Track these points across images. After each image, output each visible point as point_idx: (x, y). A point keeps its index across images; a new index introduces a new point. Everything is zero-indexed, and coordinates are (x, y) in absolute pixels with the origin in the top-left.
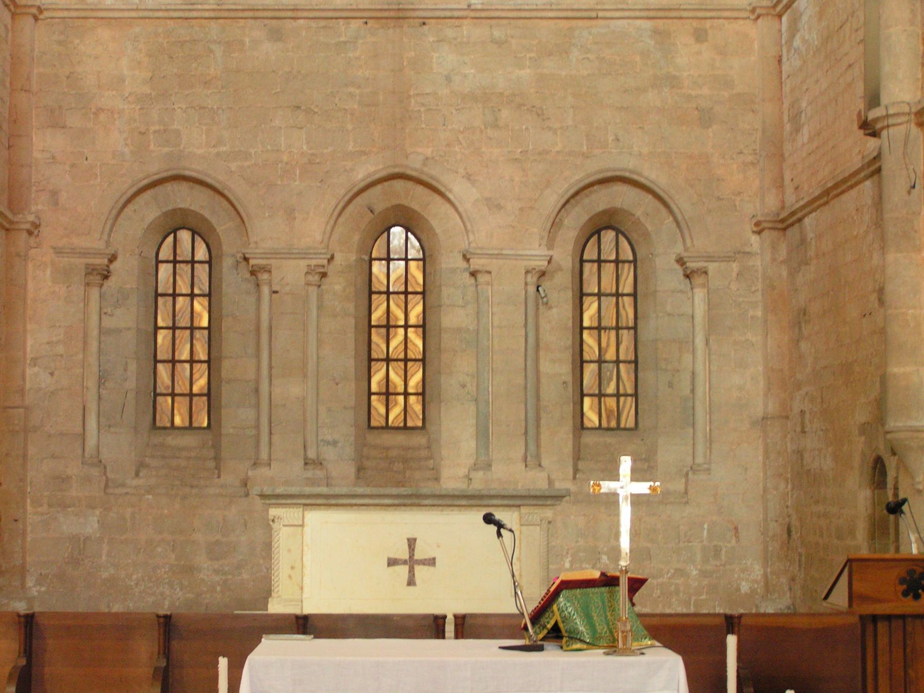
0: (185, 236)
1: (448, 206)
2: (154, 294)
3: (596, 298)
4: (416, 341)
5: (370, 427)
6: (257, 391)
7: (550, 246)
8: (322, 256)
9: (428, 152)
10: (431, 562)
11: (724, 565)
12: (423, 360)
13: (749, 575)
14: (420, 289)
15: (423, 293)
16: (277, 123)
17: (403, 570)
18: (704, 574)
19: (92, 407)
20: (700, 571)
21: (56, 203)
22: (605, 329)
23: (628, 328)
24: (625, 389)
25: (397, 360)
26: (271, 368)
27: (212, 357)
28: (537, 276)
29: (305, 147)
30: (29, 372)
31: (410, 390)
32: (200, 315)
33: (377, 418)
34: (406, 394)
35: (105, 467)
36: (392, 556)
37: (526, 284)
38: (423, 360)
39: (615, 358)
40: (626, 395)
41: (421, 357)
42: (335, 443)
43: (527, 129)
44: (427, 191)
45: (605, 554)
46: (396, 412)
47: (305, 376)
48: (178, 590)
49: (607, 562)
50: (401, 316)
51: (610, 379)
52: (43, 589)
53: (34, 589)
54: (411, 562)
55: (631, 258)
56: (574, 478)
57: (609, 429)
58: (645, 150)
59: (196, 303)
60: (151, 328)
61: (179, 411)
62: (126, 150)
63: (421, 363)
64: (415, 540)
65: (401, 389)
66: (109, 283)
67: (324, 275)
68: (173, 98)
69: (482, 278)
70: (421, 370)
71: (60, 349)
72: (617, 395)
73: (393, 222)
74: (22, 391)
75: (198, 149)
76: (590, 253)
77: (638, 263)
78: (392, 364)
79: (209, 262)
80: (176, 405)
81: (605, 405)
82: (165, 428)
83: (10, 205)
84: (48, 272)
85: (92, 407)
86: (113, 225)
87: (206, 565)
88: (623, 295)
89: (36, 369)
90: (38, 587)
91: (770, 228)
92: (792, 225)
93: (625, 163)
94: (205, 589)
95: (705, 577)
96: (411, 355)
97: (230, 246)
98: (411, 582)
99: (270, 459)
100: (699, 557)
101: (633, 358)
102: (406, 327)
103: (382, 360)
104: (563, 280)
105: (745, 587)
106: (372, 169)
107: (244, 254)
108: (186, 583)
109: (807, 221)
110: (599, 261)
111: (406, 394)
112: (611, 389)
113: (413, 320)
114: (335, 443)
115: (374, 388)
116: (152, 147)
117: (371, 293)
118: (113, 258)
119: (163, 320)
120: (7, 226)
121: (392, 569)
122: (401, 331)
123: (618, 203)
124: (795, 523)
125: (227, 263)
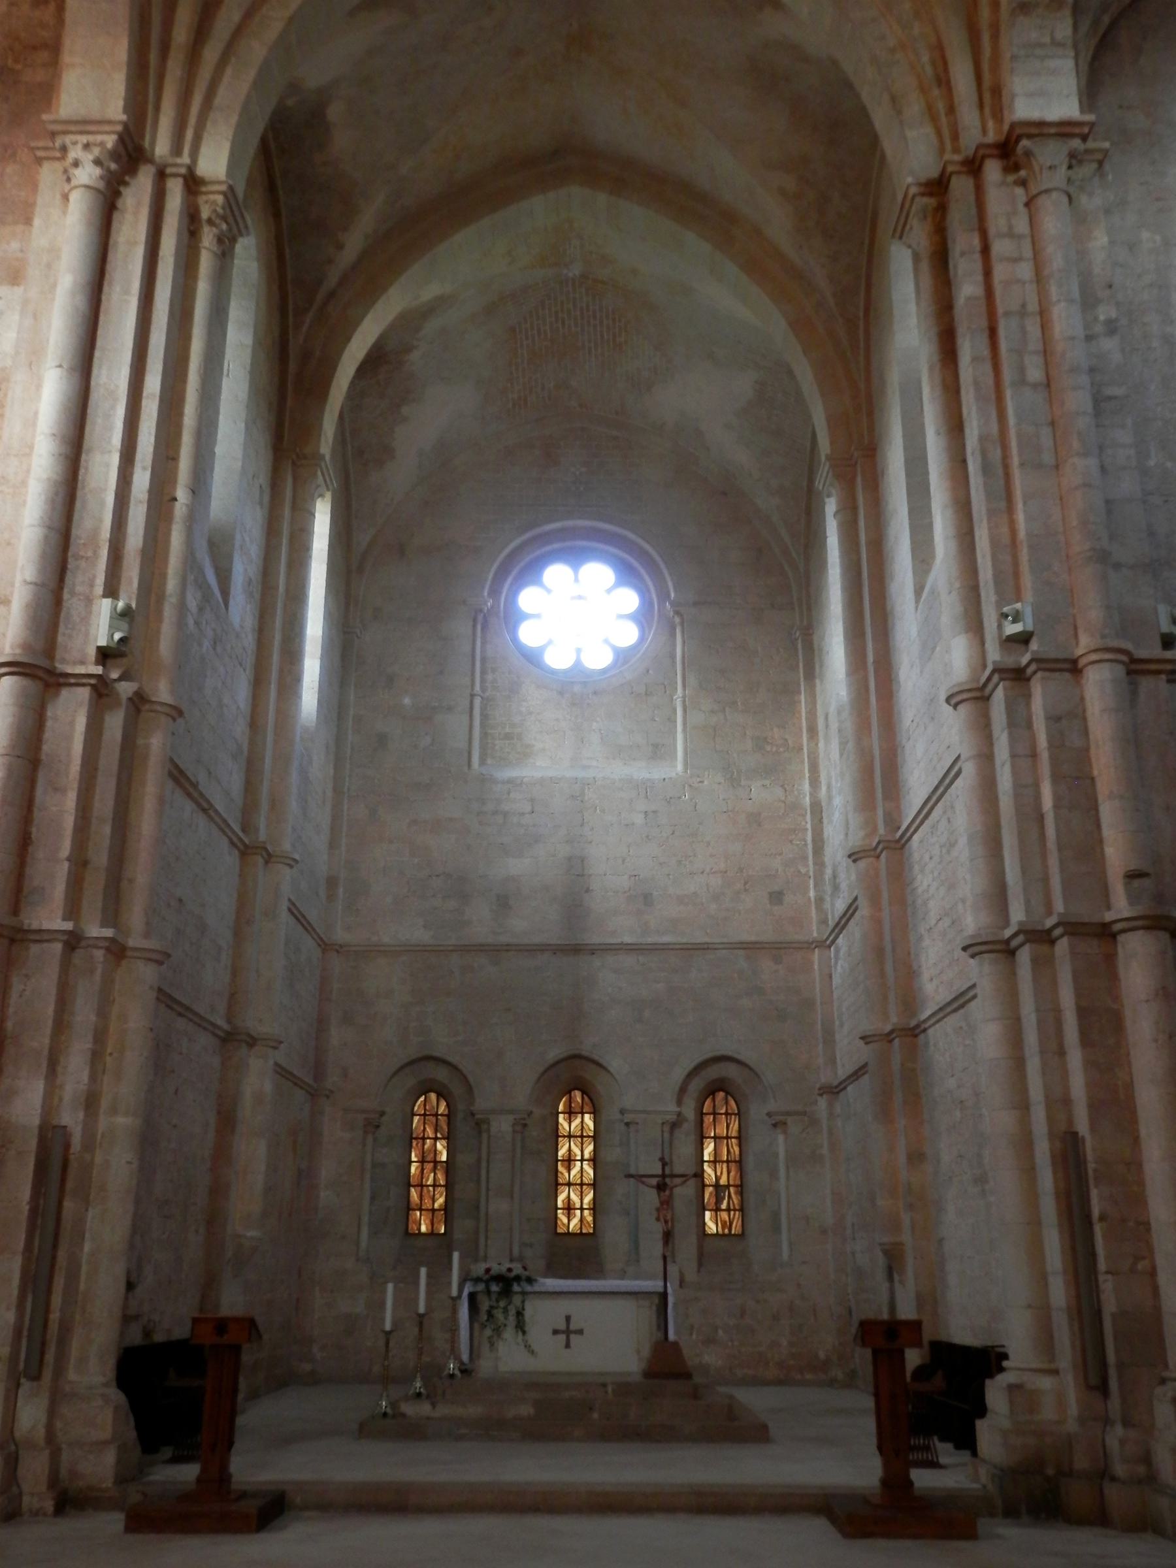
6: (477, 1208)
7: (679, 1102)
17: (563, 1337)
19: (365, 1219)
26: (488, 1189)
30: (322, 1194)
31: (585, 1206)
32: (441, 1153)
34: (582, 1209)
40: (735, 1210)
42: (531, 1245)
46: (575, 1222)
47: (512, 1197)
50: (578, 1153)
54: (568, 1332)
56: (699, 1271)
57: (724, 1235)
65: (578, 1205)
67: (525, 1125)
72: (728, 1210)
75: (443, 1042)
76: (707, 1107)
79: (448, 1116)
82: (415, 1234)
85: (365, 1219)
96: (585, 1181)
97: (461, 1107)
98: (568, 1346)
102: (582, 1160)
104: (689, 1126)
105: (822, 1355)
109: (849, 1089)
110: (715, 1114)
111: (582, 1209)
112: (724, 1206)
113: (587, 1156)
114: (531, 1245)
115: (560, 1204)
118: (382, 1114)
122: (578, 1163)
125: (460, 1116)
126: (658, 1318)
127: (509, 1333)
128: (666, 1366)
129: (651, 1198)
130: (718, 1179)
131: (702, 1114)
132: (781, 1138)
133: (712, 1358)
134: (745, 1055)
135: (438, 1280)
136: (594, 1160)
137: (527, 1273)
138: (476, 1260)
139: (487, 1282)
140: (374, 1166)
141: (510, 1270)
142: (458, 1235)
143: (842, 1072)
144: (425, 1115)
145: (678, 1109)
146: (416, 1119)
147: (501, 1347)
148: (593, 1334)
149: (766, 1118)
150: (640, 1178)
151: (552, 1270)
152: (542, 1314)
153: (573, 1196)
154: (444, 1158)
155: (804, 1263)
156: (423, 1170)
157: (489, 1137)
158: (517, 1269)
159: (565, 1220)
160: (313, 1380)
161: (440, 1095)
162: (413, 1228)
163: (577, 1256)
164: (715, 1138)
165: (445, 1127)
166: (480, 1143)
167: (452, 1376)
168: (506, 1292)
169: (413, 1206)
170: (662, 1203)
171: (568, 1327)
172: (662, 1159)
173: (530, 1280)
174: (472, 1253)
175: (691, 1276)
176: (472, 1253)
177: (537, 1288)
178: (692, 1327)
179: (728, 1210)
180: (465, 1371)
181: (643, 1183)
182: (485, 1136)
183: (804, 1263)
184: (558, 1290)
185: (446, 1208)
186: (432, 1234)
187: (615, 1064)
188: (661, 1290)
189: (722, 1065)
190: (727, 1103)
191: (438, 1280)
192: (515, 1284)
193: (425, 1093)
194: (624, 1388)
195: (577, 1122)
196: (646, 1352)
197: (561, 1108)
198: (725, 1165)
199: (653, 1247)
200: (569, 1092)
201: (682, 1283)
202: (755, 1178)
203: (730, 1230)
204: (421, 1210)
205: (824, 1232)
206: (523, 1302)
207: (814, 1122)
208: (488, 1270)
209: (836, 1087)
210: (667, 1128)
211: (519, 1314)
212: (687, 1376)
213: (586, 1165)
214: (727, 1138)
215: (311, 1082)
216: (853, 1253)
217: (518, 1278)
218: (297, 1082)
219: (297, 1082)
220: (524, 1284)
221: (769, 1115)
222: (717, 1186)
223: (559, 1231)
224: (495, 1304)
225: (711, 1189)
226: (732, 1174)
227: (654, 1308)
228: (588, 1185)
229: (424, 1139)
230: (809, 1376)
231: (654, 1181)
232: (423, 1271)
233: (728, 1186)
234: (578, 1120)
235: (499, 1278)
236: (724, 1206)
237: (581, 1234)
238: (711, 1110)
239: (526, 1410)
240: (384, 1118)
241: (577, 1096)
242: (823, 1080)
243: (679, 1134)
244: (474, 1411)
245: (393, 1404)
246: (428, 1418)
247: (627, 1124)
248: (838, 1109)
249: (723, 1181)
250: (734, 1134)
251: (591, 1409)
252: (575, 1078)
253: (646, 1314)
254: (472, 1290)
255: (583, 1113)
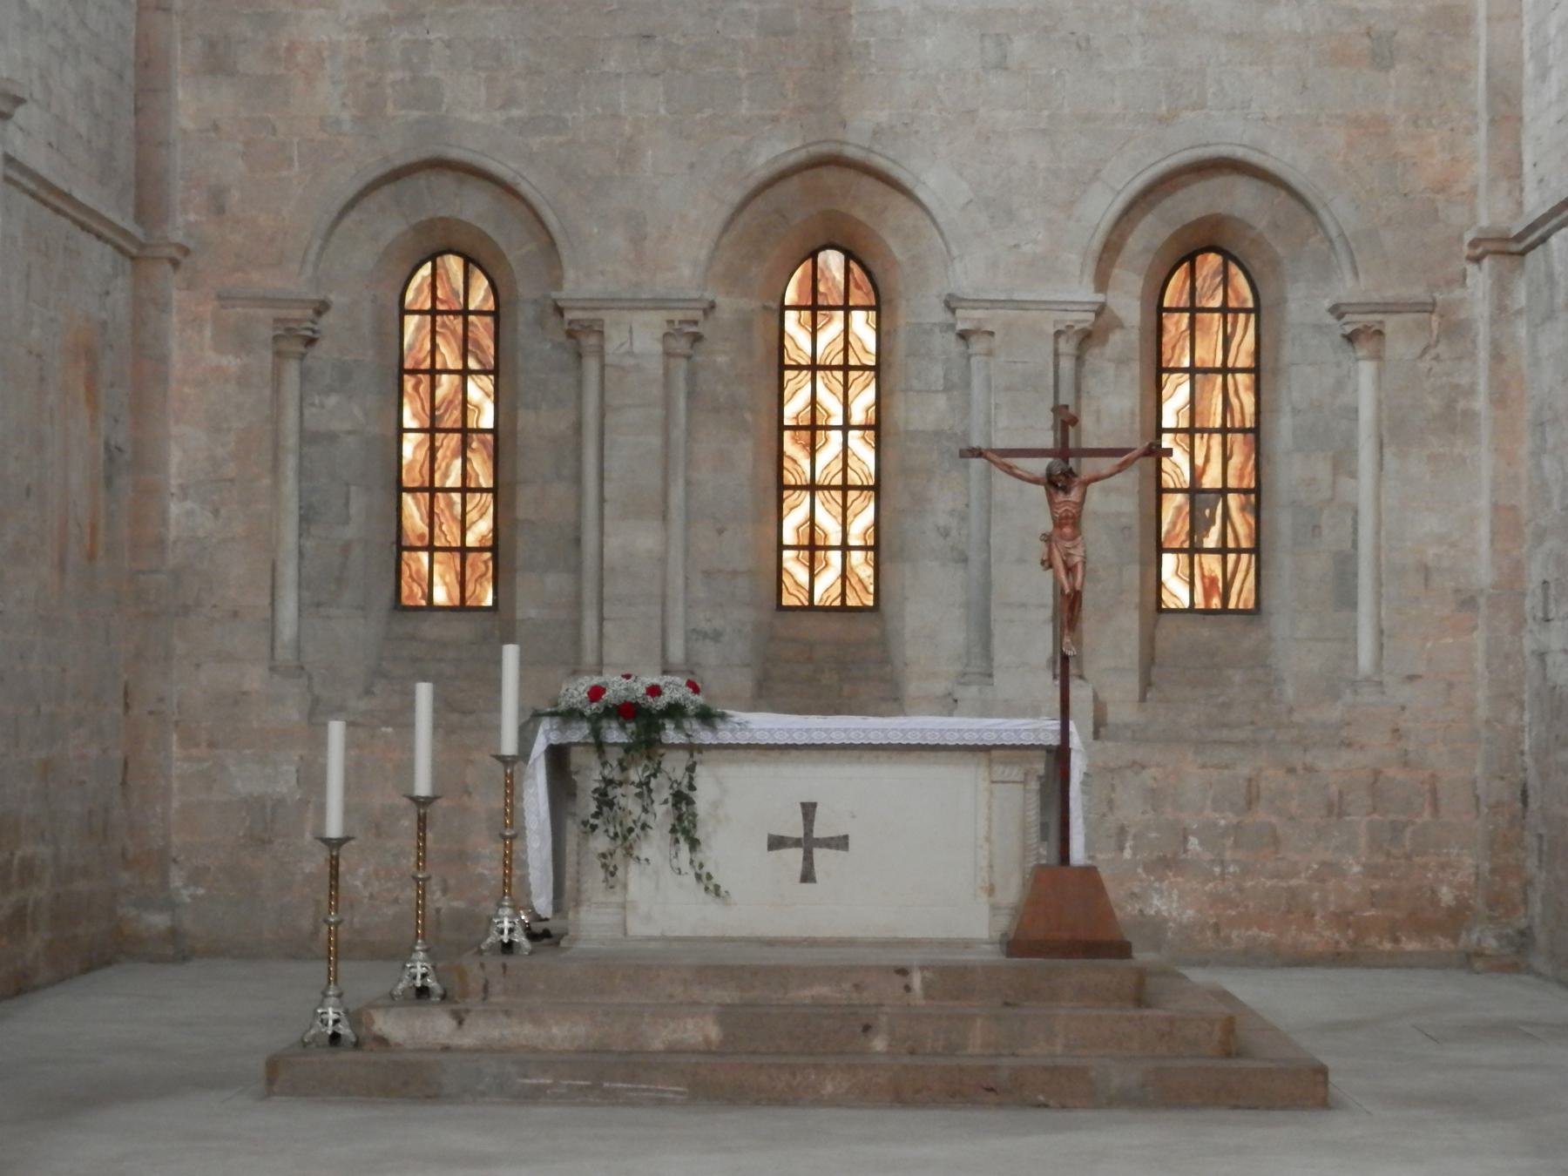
0: (453, 265)
1: (918, 212)
2: (396, 370)
3: (1187, 376)
4: (863, 453)
5: (780, 607)
6: (578, 541)
7: (1102, 281)
8: (693, 304)
9: (883, 116)
10: (841, 843)
11: (1408, 857)
12: (876, 488)
13: (1454, 874)
14: (871, 361)
15: (876, 369)
16: (612, 65)
17: (795, 856)
18: (1372, 871)
19: (289, 572)
20: (1364, 866)
21: (220, 210)
22: (1202, 431)
23: (1243, 430)
24: (1237, 538)
25: (829, 488)
26: (602, 500)
27: (500, 481)
28: (1073, 343)
29: (662, 111)
30: (175, 509)
31: (852, 542)
33: (792, 590)
34: (845, 548)
35: (310, 678)
36: (776, 832)
37: (1056, 354)
38: (876, 488)
39: (1219, 486)
40: (1239, 551)
41: (872, 483)
42: (716, 636)
43: (1059, 74)
44: (880, 187)
45: (1194, 834)
47: (665, 517)
48: (438, 894)
49: (1199, 849)
51: (1212, 521)
52: (201, 891)
53: (185, 893)
55: (1250, 304)
56: (1143, 699)
57: (1208, 612)
58: (1273, 113)
59: (471, 385)
60: (392, 432)
61: (442, 577)
62: (345, 116)
63: (872, 493)
64: (814, 805)
65: (835, 540)
66: (321, 350)
67: (697, 338)
68: (427, 22)
69: (978, 345)
70: (872, 505)
71: (231, 469)
72: (1223, 550)
73: (821, 242)
74: (160, 544)
75: (475, 121)
77: (1264, 312)
78: (819, 495)
79: (495, 314)
80: (436, 567)
81: (1202, 568)
82: (418, 608)
83: (140, 215)
84: (208, 333)
85: (289, 572)
86: (322, 248)
87: (487, 851)
88: (1235, 371)
89: (189, 505)
90: (192, 889)
91: (1496, 253)
92: (1532, 247)
93: (1232, 139)
94: (486, 893)
95: (1375, 876)
96: (853, 479)
97: (527, 290)
98: (808, 876)
99: (600, 663)
100: (1363, 841)
101: (1253, 485)
102: (846, 427)
103: (823, 488)
105: (1446, 895)
106: (783, 148)
107: (555, 301)
108: (452, 882)
109: (1554, 240)
110: (1193, 310)
111: (845, 548)
112: (1211, 540)
113: (858, 417)
114: (716, 636)
115: (789, 537)
116: (390, 109)
117: (783, 367)
118: (322, 308)
119: (415, 415)
120: (134, 251)
121: (774, 853)
123: (1222, 207)
124: (1533, 779)
126: (1044, 807)
127: (655, 846)
128: (1065, 925)
129: (1030, 509)
130: (1196, 474)
131: (1161, 309)
132: (1366, 370)
133: (1168, 903)
134: (1280, 156)
135: (465, 711)
136: (876, 427)
137: (700, 699)
138: (576, 673)
139: (595, 721)
140: (308, 437)
141: (654, 691)
142: (527, 610)
143: (1535, 203)
144: (433, 312)
145: (1100, 298)
146: (411, 322)
147: (636, 881)
148: (876, 843)
149: (1330, 320)
150: (1002, 458)
151: (765, 696)
152: (742, 802)
153: (822, 517)
154: (487, 421)
155: (1412, 678)
156: (433, 451)
157: (603, 367)
158: (675, 690)
159: (802, 576)
160: (176, 949)
161: (470, 261)
162: (413, 594)
163: (832, 660)
164: (1192, 371)
165: (488, 344)
166: (580, 383)
167: (508, 947)
168: (647, 745)
169: (410, 538)
170: (1059, 523)
171: (797, 843)
172: (1058, 409)
173: (707, 717)
174: (559, 648)
175: (1123, 711)
176: (559, 648)
177: (725, 735)
178: (1122, 831)
179: (1223, 550)
180: (540, 935)
181: (1010, 470)
182: (591, 365)
183: (1412, 678)
184: (781, 739)
185: (494, 547)
186: (462, 607)
187: (934, 180)
188: (1054, 740)
189: (1218, 183)
190: (1226, 282)
191: (465, 711)
192: (669, 726)
193: (433, 258)
194: (953, 979)
195: (831, 331)
196: (1012, 892)
197: (791, 296)
198: (1216, 439)
199: (1028, 638)
200: (814, 255)
201: (1099, 728)
202: (1292, 472)
203: (1225, 598)
204: (431, 549)
205: (1467, 603)
206: (691, 769)
207: (1456, 330)
208: (596, 693)
209: (1519, 238)
210: (1067, 347)
211: (682, 799)
212: (1122, 950)
213: (856, 557)
214: (1225, 370)
215: (128, 224)
216: (1542, 656)
217: (675, 711)
218: (88, 222)
219: (88, 222)
220: (693, 725)
221: (1337, 311)
222: (1194, 490)
223: (787, 600)
224: (616, 775)
225: (1179, 499)
226: (1235, 462)
227: (1034, 785)
228: (862, 488)
229: (433, 372)
230: (1411, 945)
231: (1039, 466)
232: (424, 692)
233: (1224, 491)
234: (837, 325)
235: (626, 711)
236: (1211, 540)
237: (844, 608)
238: (1184, 302)
239: (701, 1030)
240: (327, 320)
241: (832, 261)
242: (1484, 222)
243: (1101, 359)
244: (563, 1032)
245: (356, 1018)
246: (446, 1049)
247: (963, 336)
248: (1520, 296)
249: (1211, 479)
250: (1244, 360)
251: (867, 1028)
252: (828, 212)
253: (1015, 800)
254: (555, 739)
255: (847, 309)
